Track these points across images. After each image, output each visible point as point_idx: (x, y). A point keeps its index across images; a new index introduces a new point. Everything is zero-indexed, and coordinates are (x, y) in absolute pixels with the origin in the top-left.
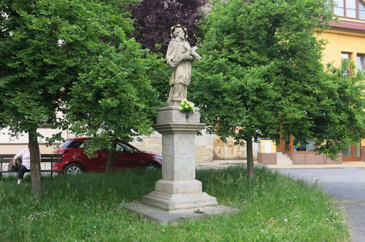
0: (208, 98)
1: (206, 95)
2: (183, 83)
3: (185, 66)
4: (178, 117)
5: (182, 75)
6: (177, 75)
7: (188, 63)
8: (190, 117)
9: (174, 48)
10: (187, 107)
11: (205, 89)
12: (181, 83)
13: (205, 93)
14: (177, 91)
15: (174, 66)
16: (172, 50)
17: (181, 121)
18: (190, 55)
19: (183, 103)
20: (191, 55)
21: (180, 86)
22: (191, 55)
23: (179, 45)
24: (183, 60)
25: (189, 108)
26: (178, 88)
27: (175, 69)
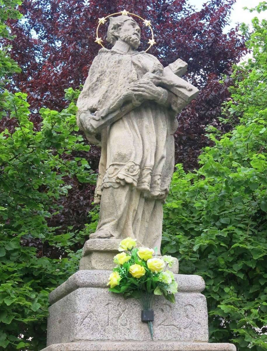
0: (249, 247)
1: (242, 239)
2: (129, 180)
3: (132, 122)
4: (103, 317)
5: (124, 152)
6: (110, 152)
7: (155, 118)
8: (159, 317)
9: (102, 73)
10: (137, 270)
11: (239, 222)
12: (123, 184)
13: (240, 233)
14: (111, 214)
15: (95, 124)
16: (95, 79)
17: (118, 336)
18: (159, 85)
19: (121, 258)
20: (161, 85)
21: (122, 195)
22: (161, 85)
23: (119, 62)
24: (126, 101)
25: (148, 274)
26: (115, 204)
27: (222, 223)
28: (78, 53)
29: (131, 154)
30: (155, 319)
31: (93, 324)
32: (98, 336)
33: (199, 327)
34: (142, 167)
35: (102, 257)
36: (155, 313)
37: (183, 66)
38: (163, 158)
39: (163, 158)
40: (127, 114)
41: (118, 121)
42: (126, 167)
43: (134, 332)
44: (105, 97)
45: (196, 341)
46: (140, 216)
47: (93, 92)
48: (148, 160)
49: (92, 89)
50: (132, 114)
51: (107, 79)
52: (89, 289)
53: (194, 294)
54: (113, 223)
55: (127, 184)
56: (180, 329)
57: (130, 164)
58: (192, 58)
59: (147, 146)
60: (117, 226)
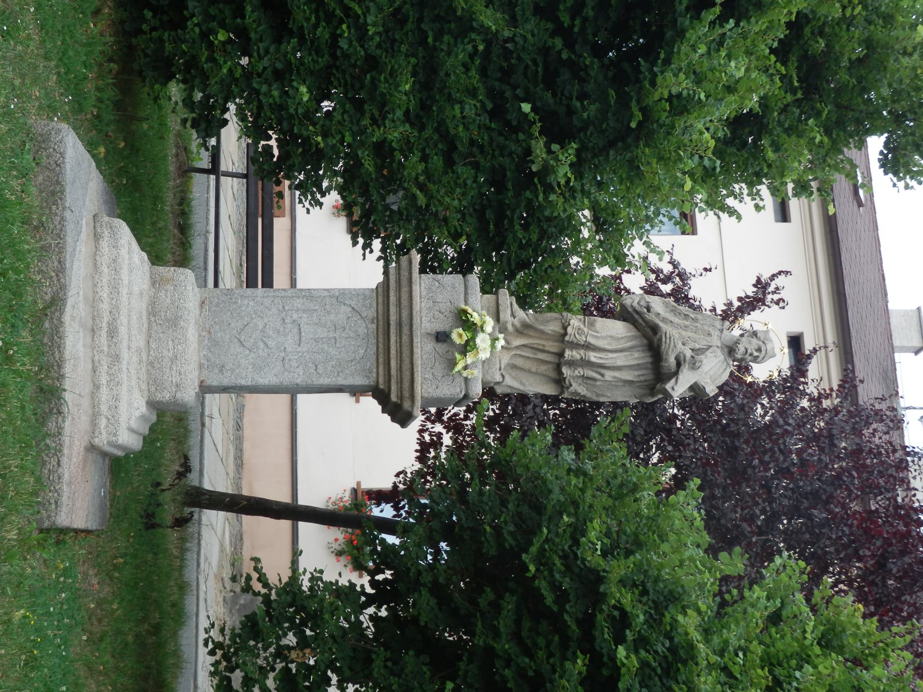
2: (569, 330)
28: (876, 496)
29: (597, 332)
30: (440, 345)
31: (434, 288)
32: (424, 293)
33: (434, 387)
34: (588, 347)
35: (493, 304)
36: (445, 345)
37: (708, 390)
38: (602, 375)
39: (602, 375)
40: (645, 336)
41: (636, 327)
42: (582, 326)
43: (428, 325)
44: (664, 320)
45: (422, 383)
46: (541, 356)
47: (672, 311)
48: (594, 354)
49: (674, 311)
50: (645, 341)
51: (687, 323)
52: (463, 286)
53: (463, 386)
54: (528, 320)
55: (565, 328)
56: (432, 368)
57: (586, 330)
58: (532, 109)
59: (611, 355)
60: (526, 326)
